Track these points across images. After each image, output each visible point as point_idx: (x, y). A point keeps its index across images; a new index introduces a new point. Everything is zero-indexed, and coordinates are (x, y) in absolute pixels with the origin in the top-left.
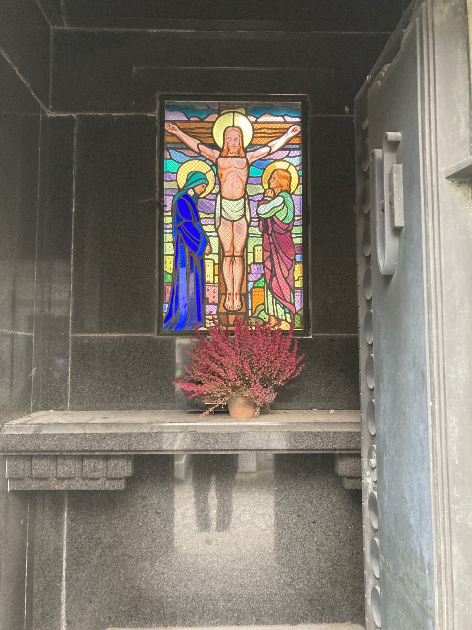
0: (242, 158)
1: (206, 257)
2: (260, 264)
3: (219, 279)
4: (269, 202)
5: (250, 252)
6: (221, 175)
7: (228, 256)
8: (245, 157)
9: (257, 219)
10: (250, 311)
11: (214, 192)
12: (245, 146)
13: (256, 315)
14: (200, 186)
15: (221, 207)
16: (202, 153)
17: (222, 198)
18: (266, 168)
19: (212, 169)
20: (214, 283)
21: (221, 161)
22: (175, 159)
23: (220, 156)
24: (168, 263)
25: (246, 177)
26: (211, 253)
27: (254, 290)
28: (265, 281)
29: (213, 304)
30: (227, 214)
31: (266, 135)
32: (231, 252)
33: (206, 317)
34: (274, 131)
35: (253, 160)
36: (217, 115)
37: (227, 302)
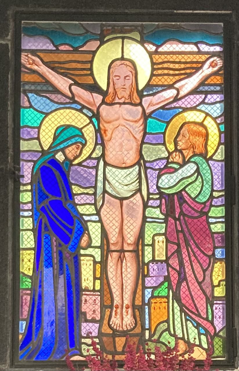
0: (136, 105)
1: (82, 252)
2: (162, 261)
4: (176, 170)
5: (148, 245)
6: (105, 131)
8: (140, 104)
9: (158, 196)
11: (94, 155)
13: (156, 337)
14: (74, 146)
15: (105, 178)
16: (76, 99)
17: (106, 164)
19: (91, 122)
20: (94, 290)
22: (36, 107)
23: (103, 102)
27: (153, 301)
28: (169, 287)
29: (93, 321)
31: (171, 72)
32: (120, 244)
33: (83, 340)
34: (183, 66)
36: (99, 43)
37: (113, 319)
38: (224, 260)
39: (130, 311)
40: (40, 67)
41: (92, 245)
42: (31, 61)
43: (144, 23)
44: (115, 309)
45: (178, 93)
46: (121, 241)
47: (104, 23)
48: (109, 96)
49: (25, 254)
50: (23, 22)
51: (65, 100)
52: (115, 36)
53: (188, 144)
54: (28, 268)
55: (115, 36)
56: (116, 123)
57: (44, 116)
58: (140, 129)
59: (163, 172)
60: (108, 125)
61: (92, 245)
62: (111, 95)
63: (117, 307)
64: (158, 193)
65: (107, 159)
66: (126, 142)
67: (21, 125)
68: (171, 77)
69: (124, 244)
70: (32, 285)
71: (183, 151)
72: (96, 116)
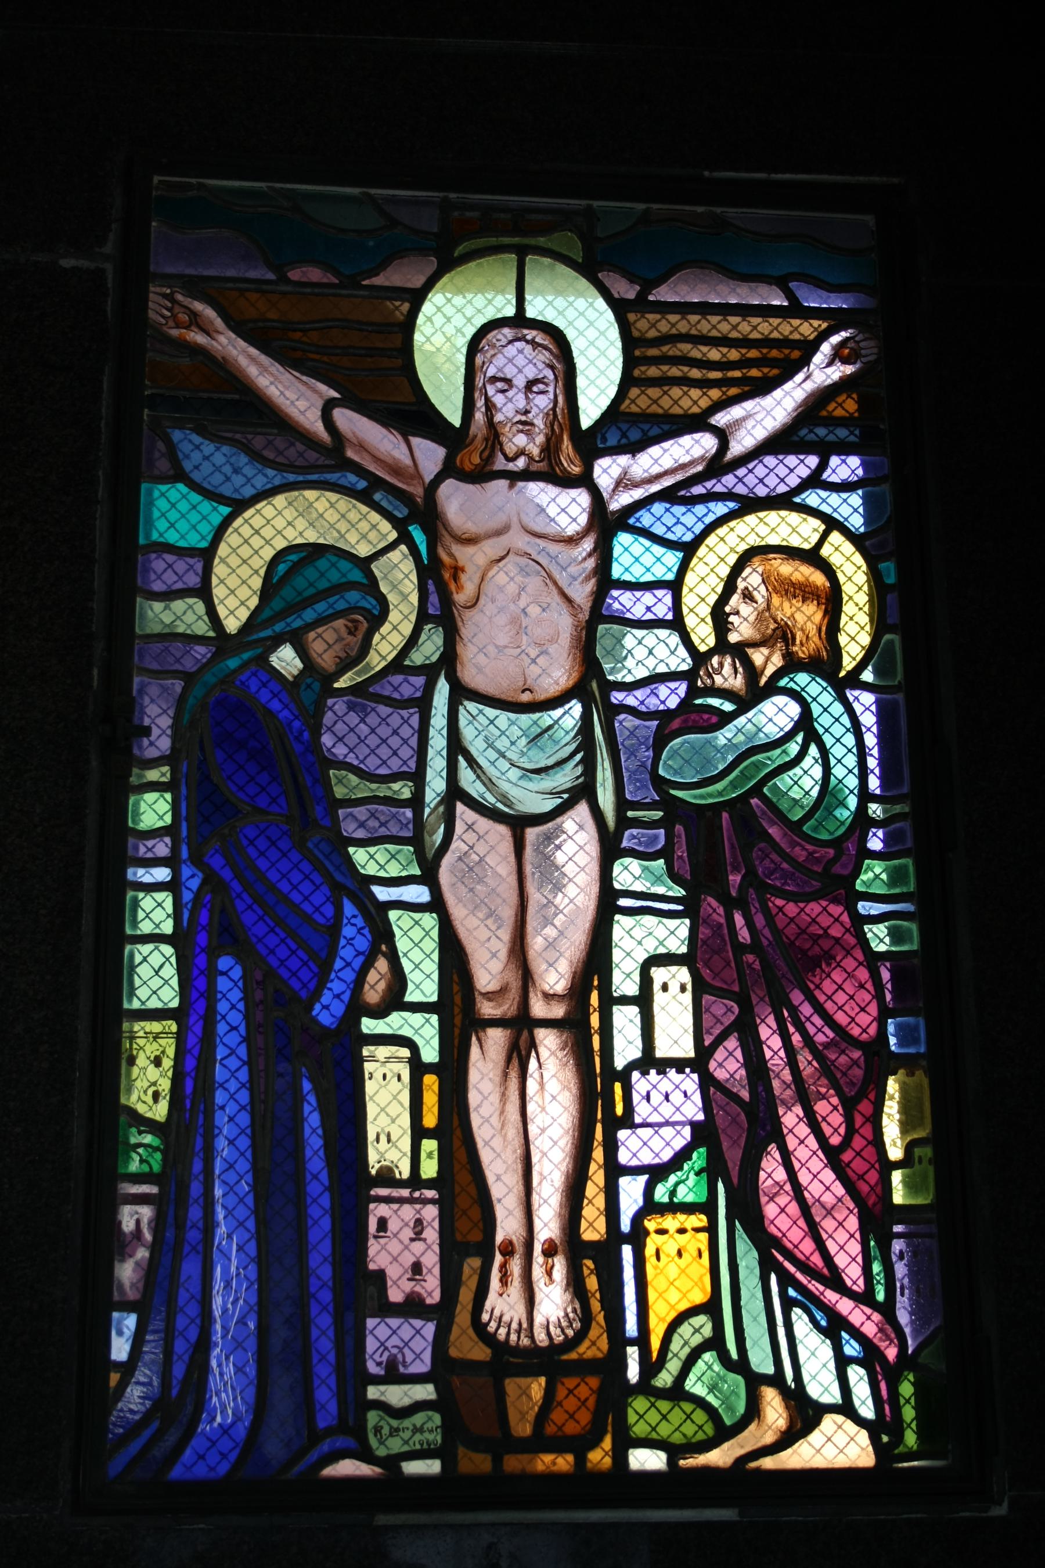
0: (566, 482)
1: (369, 1025)
2: (680, 1065)
3: (444, 1157)
4: (726, 718)
5: (625, 1000)
6: (457, 570)
7: (494, 1023)
8: (586, 481)
9: (658, 814)
10: (633, 1353)
11: (417, 658)
12: (586, 423)
13: (664, 1379)
14: (340, 623)
15: (456, 746)
16: (350, 454)
17: (460, 693)
18: (699, 539)
19: (405, 538)
20: (415, 1180)
21: (457, 501)
22: (196, 476)
23: (449, 470)
24: (141, 1061)
25: (591, 585)
26: (395, 999)
27: (650, 1225)
28: (713, 1171)
29: (413, 1307)
30: (490, 784)
31: (695, 373)
32: (514, 993)
33: (373, 1392)
34: (734, 355)
35: (625, 499)
36: (432, 264)
37: (492, 1300)
38: (924, 1063)
39: (560, 1266)
40: (215, 335)
41: (409, 998)
42: (184, 317)
43: (596, 204)
44: (498, 1259)
45: (724, 445)
46: (515, 985)
47: (453, 196)
48: (471, 448)
49: (141, 1034)
50: (156, 179)
51: (301, 454)
52: (493, 241)
53: (767, 628)
54: (150, 1092)
55: (493, 241)
56: (504, 541)
57: (225, 510)
58: (584, 569)
59: (676, 724)
60: (470, 550)
61: (409, 998)
62: (479, 444)
63: (508, 1250)
64: (655, 802)
65: (471, 675)
66: (534, 610)
67: (142, 541)
68: (695, 393)
69: (531, 995)
70: (164, 1160)
71: (750, 651)
72: (417, 514)
